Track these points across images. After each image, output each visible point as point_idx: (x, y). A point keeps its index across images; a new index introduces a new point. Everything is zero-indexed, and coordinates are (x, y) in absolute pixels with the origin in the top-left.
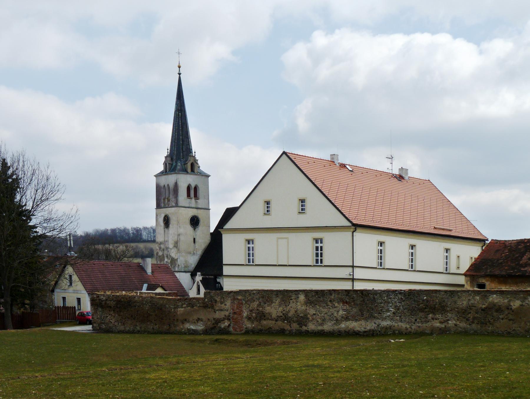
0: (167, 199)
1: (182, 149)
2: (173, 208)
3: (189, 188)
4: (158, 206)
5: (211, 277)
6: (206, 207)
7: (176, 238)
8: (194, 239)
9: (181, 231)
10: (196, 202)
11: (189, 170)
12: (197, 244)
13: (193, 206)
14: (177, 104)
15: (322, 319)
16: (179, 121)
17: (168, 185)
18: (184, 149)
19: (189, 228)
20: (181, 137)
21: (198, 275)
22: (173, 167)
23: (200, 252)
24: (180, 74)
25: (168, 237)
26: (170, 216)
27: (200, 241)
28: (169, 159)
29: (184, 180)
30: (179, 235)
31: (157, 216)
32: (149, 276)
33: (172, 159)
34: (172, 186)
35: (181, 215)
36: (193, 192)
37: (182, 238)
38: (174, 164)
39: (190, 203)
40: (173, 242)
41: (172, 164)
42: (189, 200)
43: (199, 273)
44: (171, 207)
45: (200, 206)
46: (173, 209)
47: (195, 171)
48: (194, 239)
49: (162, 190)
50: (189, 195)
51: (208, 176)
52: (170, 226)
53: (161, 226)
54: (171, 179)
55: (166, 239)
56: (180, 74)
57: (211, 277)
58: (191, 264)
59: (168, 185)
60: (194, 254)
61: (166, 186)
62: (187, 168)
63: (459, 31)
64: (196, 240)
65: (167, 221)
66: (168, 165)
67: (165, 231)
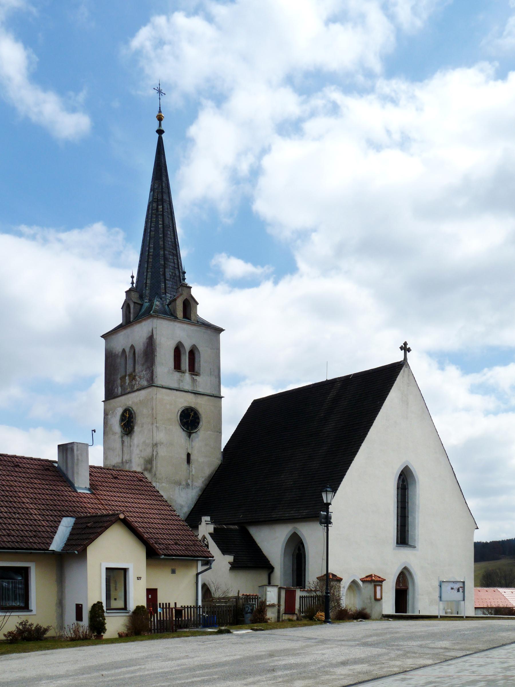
0: (130, 375)
1: (164, 274)
2: (143, 393)
3: (178, 351)
4: (110, 394)
5: (232, 527)
6: (215, 393)
7: (148, 452)
8: (189, 455)
9: (161, 436)
10: (194, 381)
11: (180, 313)
12: (193, 465)
13: (187, 387)
14: (152, 189)
15: (189, 634)
16: (157, 222)
17: (132, 347)
18: (168, 276)
19: (178, 433)
20: (162, 253)
21: (203, 523)
22: (143, 310)
23: (199, 483)
24: (160, 132)
25: (131, 453)
26: (135, 409)
27: (201, 460)
28: (135, 296)
29: (169, 334)
30: (155, 445)
31: (106, 414)
32: (81, 496)
33: (141, 297)
34: (140, 347)
35: (161, 403)
36: (187, 360)
37: (162, 452)
38: (146, 305)
39: (180, 381)
40: (142, 461)
41: (142, 305)
42: (177, 375)
43: (206, 519)
44: (138, 390)
45: (201, 390)
46: (143, 393)
47: (193, 317)
48: (189, 455)
49: (118, 360)
50: (177, 366)
51: (222, 330)
52: (136, 429)
53: (114, 434)
54: (139, 333)
55: (126, 457)
56: (160, 132)
57: (232, 527)
58: (182, 506)
59: (132, 347)
60: (188, 485)
61: (127, 350)
62: (175, 310)
63: (225, 524)
64: (192, 457)
65: (128, 422)
66: (132, 306)
67: (123, 442)
